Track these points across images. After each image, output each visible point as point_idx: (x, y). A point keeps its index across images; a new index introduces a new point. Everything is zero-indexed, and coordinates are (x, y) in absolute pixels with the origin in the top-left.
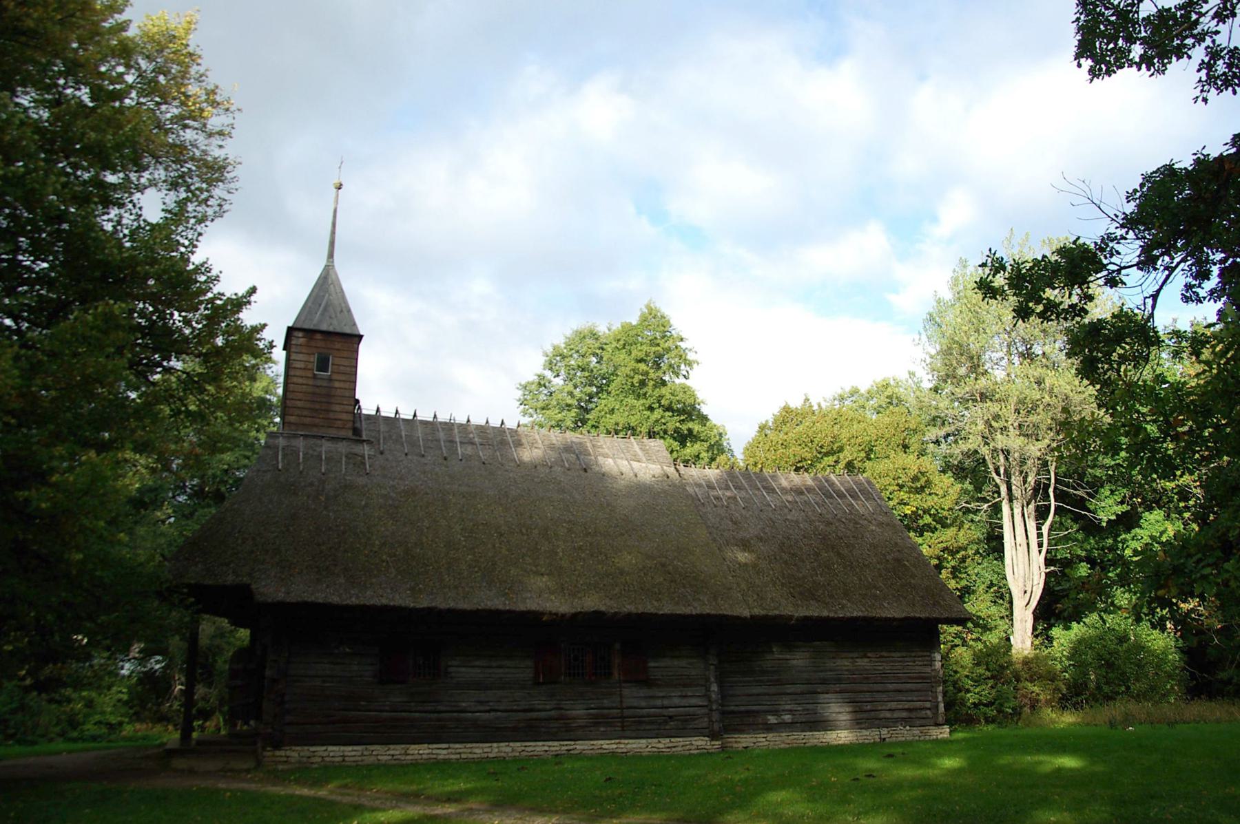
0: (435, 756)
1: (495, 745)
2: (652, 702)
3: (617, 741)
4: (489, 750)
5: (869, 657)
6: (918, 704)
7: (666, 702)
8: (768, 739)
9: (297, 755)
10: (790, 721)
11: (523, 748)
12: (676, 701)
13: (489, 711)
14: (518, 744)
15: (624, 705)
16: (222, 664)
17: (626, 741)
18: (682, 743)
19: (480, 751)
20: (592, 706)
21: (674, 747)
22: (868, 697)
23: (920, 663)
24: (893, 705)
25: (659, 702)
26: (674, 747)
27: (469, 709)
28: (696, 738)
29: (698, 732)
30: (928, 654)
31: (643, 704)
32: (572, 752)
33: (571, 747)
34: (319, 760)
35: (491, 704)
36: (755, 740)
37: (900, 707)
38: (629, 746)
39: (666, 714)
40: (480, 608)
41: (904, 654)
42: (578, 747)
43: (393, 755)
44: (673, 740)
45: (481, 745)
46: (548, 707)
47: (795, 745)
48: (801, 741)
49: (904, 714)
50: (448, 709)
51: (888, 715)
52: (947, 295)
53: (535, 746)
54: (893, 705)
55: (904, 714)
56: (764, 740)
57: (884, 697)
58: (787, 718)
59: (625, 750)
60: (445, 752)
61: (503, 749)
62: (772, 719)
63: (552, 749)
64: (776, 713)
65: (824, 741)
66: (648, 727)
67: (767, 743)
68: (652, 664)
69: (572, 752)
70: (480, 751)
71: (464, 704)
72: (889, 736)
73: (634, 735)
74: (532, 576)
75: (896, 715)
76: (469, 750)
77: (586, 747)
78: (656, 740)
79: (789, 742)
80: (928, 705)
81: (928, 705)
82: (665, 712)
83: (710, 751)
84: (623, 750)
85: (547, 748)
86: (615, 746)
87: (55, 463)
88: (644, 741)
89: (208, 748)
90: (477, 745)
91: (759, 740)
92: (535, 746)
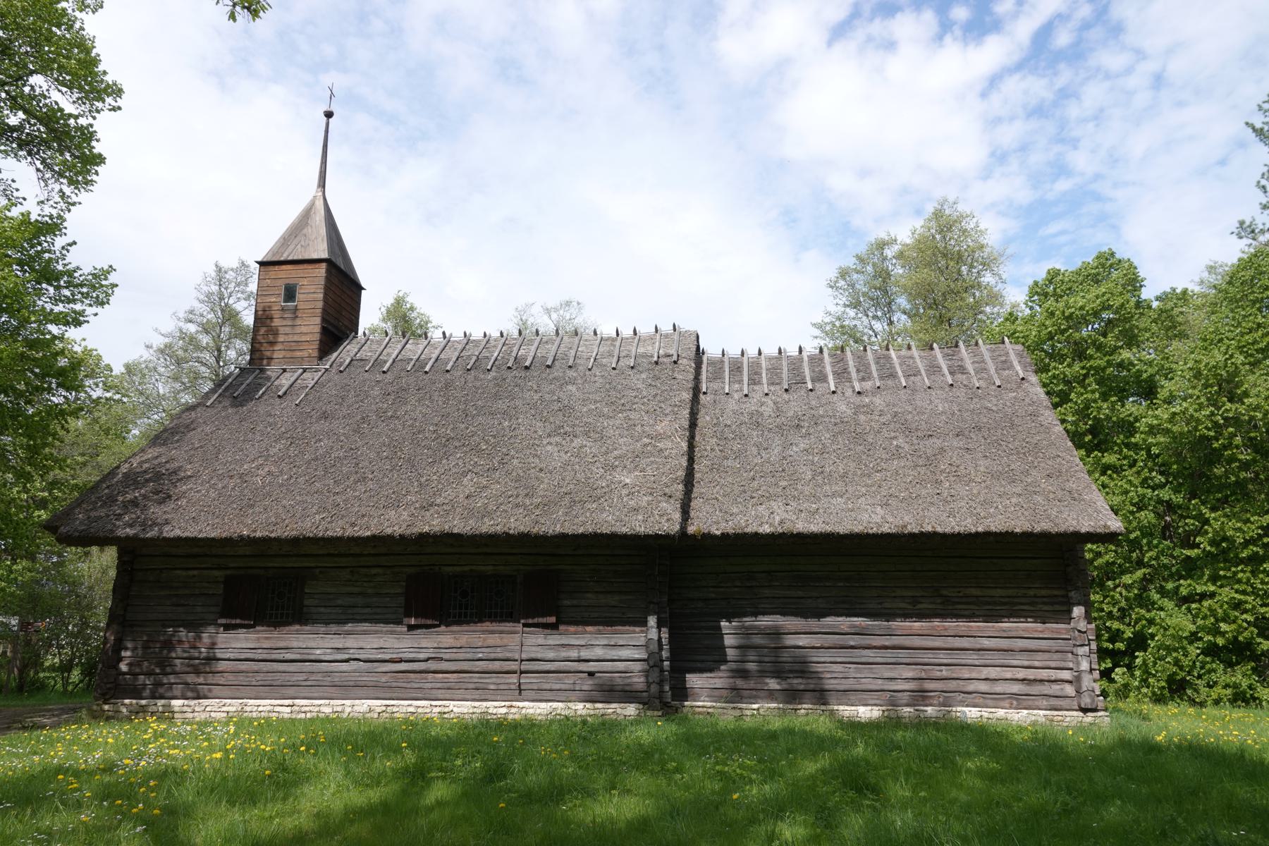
1: (348, 702)
2: (564, 654)
4: (339, 709)
5: (941, 596)
7: (585, 654)
11: (384, 708)
12: (599, 652)
13: (347, 661)
15: (524, 656)
20: (480, 655)
22: (943, 657)
24: (993, 673)
25: (574, 654)
27: (323, 658)
33: (446, 710)
35: (351, 651)
37: (1009, 675)
41: (1010, 592)
42: (455, 710)
43: (228, 712)
45: (332, 702)
46: (422, 656)
49: (1016, 688)
51: (983, 687)
54: (993, 673)
55: (1016, 688)
57: (972, 658)
60: (288, 709)
68: (567, 602)
71: (318, 652)
75: (999, 688)
80: (1066, 675)
81: (1066, 675)
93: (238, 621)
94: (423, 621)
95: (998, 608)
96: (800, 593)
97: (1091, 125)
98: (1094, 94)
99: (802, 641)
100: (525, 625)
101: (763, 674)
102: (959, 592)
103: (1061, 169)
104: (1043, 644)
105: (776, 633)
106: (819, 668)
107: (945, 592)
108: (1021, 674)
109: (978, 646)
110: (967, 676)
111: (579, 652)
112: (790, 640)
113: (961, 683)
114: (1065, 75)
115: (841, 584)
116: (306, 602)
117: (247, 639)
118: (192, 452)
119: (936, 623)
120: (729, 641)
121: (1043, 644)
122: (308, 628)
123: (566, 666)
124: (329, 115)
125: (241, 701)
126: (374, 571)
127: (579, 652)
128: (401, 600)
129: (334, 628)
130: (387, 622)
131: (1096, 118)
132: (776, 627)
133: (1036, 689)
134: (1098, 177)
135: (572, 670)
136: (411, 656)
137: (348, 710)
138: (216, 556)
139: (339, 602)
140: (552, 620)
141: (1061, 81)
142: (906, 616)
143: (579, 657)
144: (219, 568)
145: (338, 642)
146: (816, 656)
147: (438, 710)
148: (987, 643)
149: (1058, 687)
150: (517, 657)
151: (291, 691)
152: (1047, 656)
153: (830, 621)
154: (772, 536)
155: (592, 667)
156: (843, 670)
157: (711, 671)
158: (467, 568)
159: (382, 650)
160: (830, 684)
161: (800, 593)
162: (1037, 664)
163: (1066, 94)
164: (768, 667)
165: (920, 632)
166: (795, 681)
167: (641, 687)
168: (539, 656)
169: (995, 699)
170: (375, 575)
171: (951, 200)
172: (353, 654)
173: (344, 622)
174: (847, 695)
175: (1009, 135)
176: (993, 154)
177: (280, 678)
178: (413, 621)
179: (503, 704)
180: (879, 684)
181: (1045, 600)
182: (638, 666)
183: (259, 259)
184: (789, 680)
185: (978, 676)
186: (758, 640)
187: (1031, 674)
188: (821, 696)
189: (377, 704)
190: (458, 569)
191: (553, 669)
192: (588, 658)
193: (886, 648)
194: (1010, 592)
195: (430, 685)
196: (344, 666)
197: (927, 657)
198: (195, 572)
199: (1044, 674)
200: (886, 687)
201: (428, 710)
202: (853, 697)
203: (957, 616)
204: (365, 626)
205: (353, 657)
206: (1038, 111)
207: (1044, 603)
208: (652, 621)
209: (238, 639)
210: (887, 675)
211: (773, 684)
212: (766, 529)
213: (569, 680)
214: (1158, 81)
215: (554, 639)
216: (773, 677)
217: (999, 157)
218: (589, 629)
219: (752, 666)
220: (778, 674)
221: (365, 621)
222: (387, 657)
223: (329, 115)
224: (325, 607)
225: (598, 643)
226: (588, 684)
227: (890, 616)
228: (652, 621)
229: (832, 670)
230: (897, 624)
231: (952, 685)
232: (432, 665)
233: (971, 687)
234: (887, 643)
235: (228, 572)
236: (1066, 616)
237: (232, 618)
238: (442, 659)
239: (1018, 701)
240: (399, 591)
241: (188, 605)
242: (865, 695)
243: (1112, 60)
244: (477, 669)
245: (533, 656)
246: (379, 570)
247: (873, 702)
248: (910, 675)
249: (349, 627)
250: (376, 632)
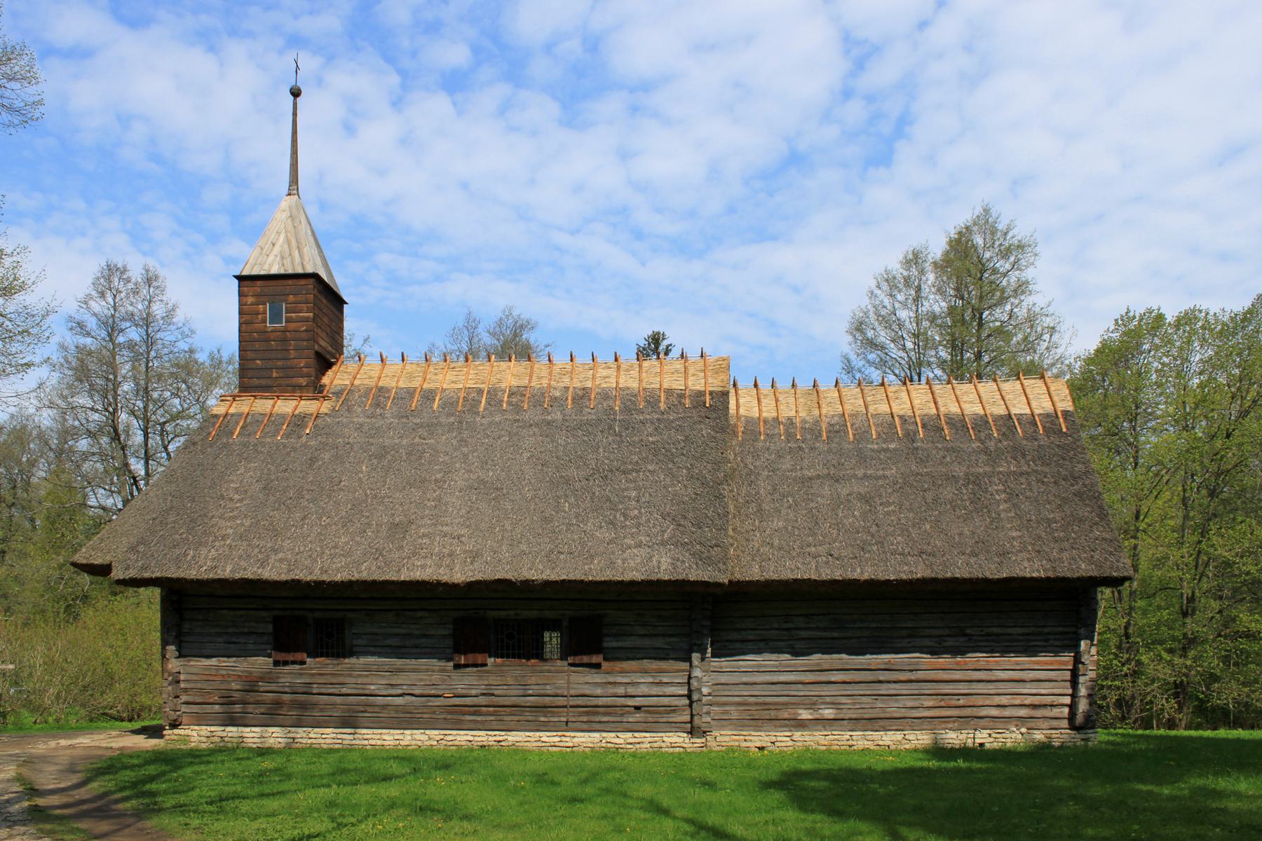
0: (340, 741)
2: (612, 690)
3: (560, 733)
5: (966, 635)
7: (631, 690)
8: (794, 738)
9: (196, 735)
10: (832, 717)
11: (442, 737)
12: (644, 689)
14: (436, 732)
15: (572, 692)
17: (572, 734)
18: (650, 740)
19: (392, 738)
20: (530, 692)
21: (639, 743)
22: (962, 688)
23: (1057, 643)
24: (1004, 700)
25: (621, 690)
26: (639, 743)
27: (377, 692)
28: (668, 734)
29: (675, 727)
30: (1073, 629)
31: (599, 691)
32: (502, 743)
33: (501, 738)
34: (218, 740)
35: (405, 687)
36: (774, 739)
37: (1017, 702)
38: (575, 740)
39: (629, 703)
40: (353, 579)
42: (510, 738)
43: (294, 738)
44: (636, 734)
45: (392, 731)
46: (473, 692)
47: (835, 747)
48: (845, 743)
49: (1023, 712)
53: (455, 735)
55: (1023, 712)
56: (788, 739)
57: (990, 688)
58: (828, 713)
59: (571, 745)
60: (351, 737)
61: (417, 737)
62: (805, 714)
63: (476, 739)
64: (812, 706)
65: (881, 743)
66: (605, 719)
67: (791, 743)
69: (502, 743)
70: (392, 738)
71: (373, 687)
72: (991, 740)
73: (585, 726)
75: (1007, 712)
76: (379, 737)
77: (520, 739)
78: (613, 734)
79: (826, 743)
82: (631, 702)
83: (689, 750)
84: (567, 744)
85: (471, 738)
86: (559, 739)
87: (1018, 533)
88: (597, 735)
90: (387, 731)
91: (779, 739)
92: (455, 735)
95: (1015, 644)
96: (835, 635)
100: (571, 665)
102: (982, 631)
107: (968, 631)
108: (1029, 700)
109: (993, 678)
110: (980, 703)
111: (626, 689)
113: (974, 709)
115: (874, 625)
118: (1242, 459)
123: (614, 701)
124: (296, 93)
125: (305, 729)
126: (420, 614)
127: (626, 689)
128: (450, 642)
133: (1039, 713)
135: (619, 704)
139: (389, 642)
140: (596, 659)
143: (626, 693)
144: (265, 609)
149: (1058, 710)
150: (565, 693)
152: (1052, 684)
156: (871, 701)
159: (435, 687)
161: (835, 635)
162: (1043, 691)
165: (943, 667)
166: (827, 711)
168: (587, 692)
170: (421, 618)
172: (405, 689)
179: (555, 734)
181: (1057, 636)
183: (238, 274)
184: (820, 711)
187: (1036, 700)
191: (600, 704)
192: (633, 694)
193: (911, 681)
196: (399, 701)
198: (243, 612)
199: (1049, 699)
200: (907, 715)
201: (484, 739)
205: (407, 692)
207: (1055, 640)
215: (597, 678)
216: (805, 709)
223: (296, 93)
224: (374, 646)
225: (643, 681)
233: (984, 712)
234: (913, 678)
235: (276, 613)
238: (493, 695)
240: (446, 632)
241: (239, 643)
244: (528, 704)
247: (894, 728)
248: (931, 704)
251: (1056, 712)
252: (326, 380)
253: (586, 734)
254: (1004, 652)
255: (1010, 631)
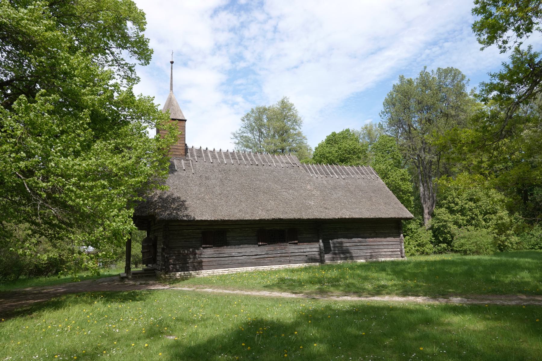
2: (300, 251)
4: (243, 270)
6: (395, 250)
7: (305, 250)
12: (308, 250)
16: (125, 252)
22: (376, 247)
25: (302, 251)
27: (235, 255)
31: (297, 251)
41: (389, 231)
45: (240, 268)
46: (263, 253)
49: (390, 253)
50: (228, 256)
51: (384, 253)
52: (324, 141)
55: (390, 253)
57: (382, 247)
60: (228, 271)
68: (299, 237)
74: (534, 266)
80: (399, 250)
81: (399, 250)
82: (304, 254)
89: (137, 276)
93: (208, 246)
94: (263, 244)
97: (253, 41)
98: (254, 29)
99: (348, 245)
100: (289, 243)
101: (339, 253)
103: (241, 57)
104: (395, 243)
105: (341, 243)
106: (352, 251)
112: (345, 245)
114: (244, 17)
116: (228, 239)
117: (211, 251)
119: (375, 239)
120: (332, 245)
121: (395, 243)
122: (229, 247)
124: (172, 63)
126: (247, 229)
129: (237, 247)
130: (252, 244)
131: (254, 38)
132: (341, 242)
134: (254, 64)
136: (260, 253)
137: (245, 270)
138: (197, 225)
139: (238, 239)
140: (296, 242)
141: (242, 19)
142: (369, 238)
145: (240, 250)
146: (350, 248)
147: (270, 268)
148: (385, 243)
151: (227, 266)
153: (353, 239)
154: (349, 219)
155: (307, 254)
157: (328, 253)
158: (272, 228)
160: (354, 255)
163: (243, 25)
164: (340, 252)
167: (318, 258)
169: (386, 256)
171: (287, 97)
172: (244, 254)
173: (240, 245)
174: (358, 257)
175: (224, 37)
176: (216, 44)
177: (222, 262)
178: (260, 244)
180: (364, 254)
182: (317, 253)
185: (385, 250)
186: (338, 245)
188: (352, 258)
189: (253, 268)
190: (270, 228)
193: (365, 245)
194: (389, 231)
195: (266, 262)
197: (373, 247)
202: (359, 258)
203: (379, 237)
204: (246, 246)
206: (232, 30)
208: (321, 241)
209: (208, 251)
210: (366, 252)
211: (342, 256)
212: (347, 217)
213: (302, 258)
214: (275, 29)
215: (297, 247)
217: (218, 47)
218: (305, 244)
219: (337, 252)
220: (343, 253)
221: (246, 244)
222: (254, 254)
223: (172, 63)
226: (306, 258)
227: (366, 238)
228: (321, 241)
229: (355, 252)
230: (368, 240)
231: (378, 253)
232: (266, 256)
236: (399, 236)
237: (207, 245)
238: (268, 254)
239: (390, 256)
242: (361, 257)
243: (259, 16)
245: (292, 252)
246: (248, 229)
248: (370, 252)
249: (241, 246)
250: (250, 247)
251: (397, 253)
252: (156, 128)
253: (295, 265)
254: (385, 237)
255: (385, 231)
